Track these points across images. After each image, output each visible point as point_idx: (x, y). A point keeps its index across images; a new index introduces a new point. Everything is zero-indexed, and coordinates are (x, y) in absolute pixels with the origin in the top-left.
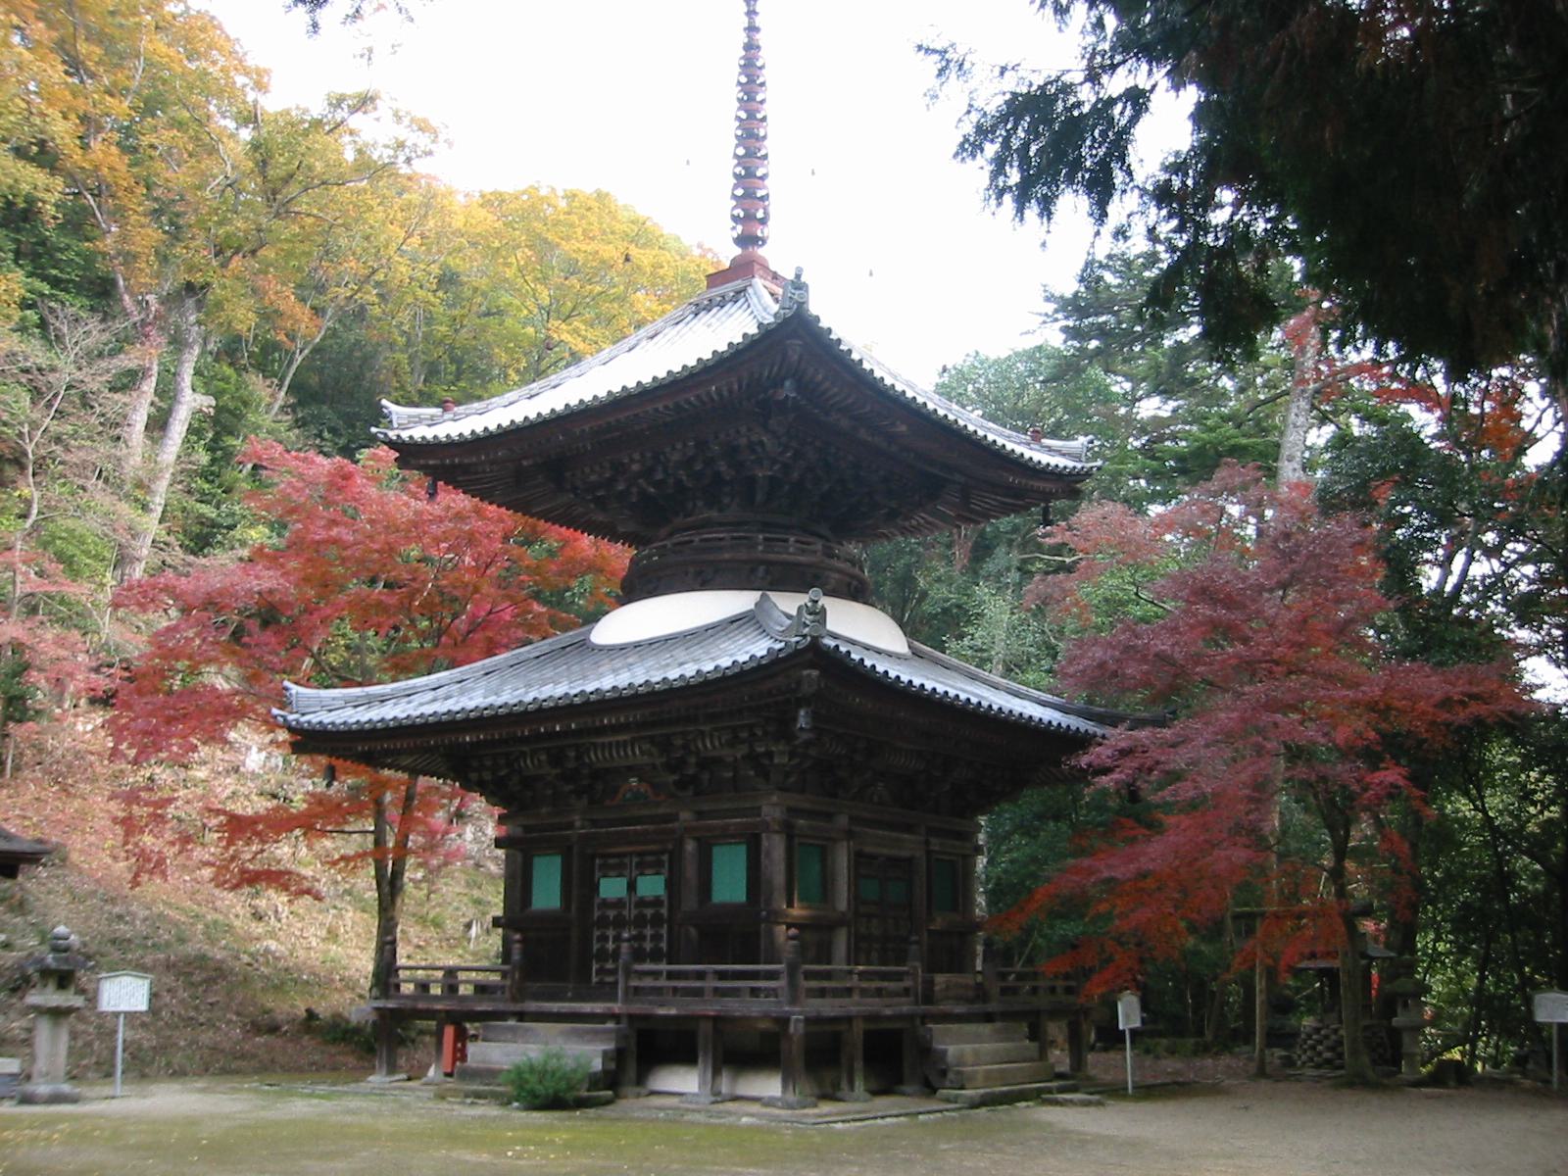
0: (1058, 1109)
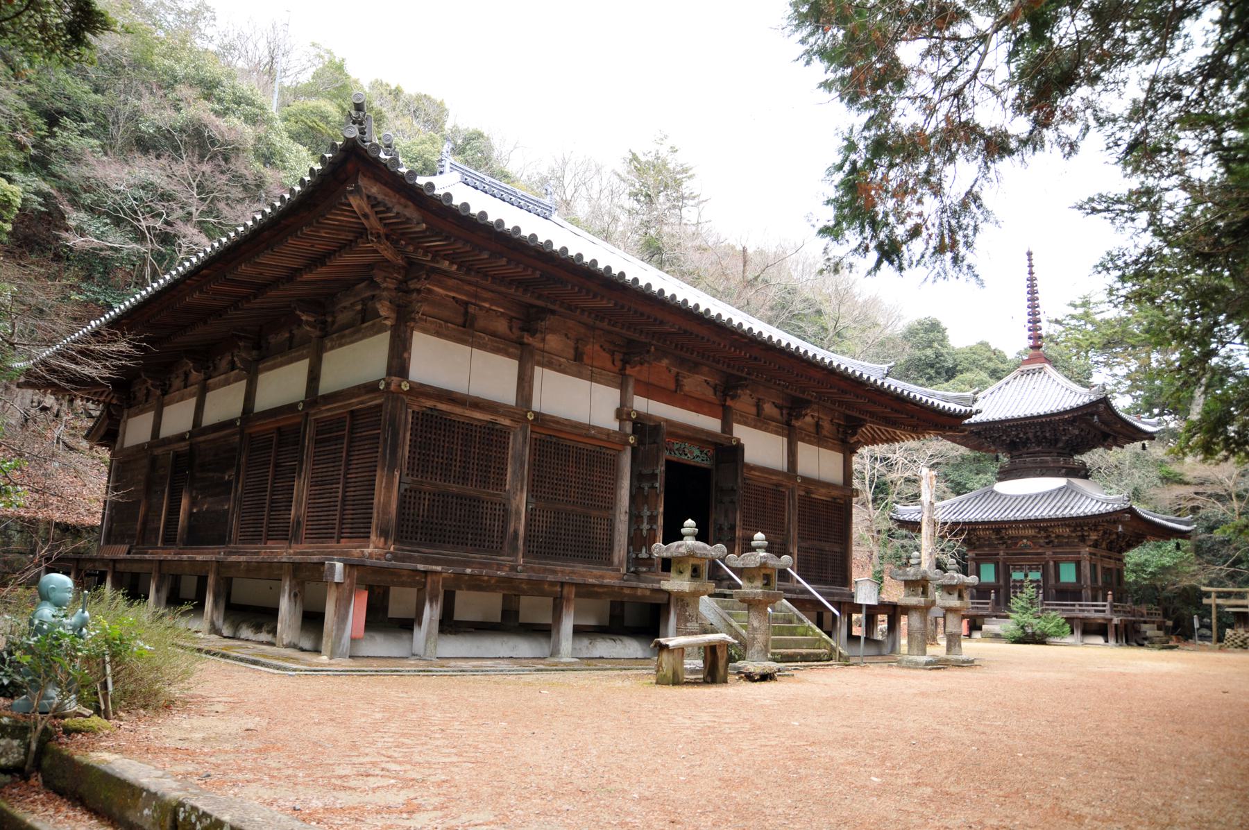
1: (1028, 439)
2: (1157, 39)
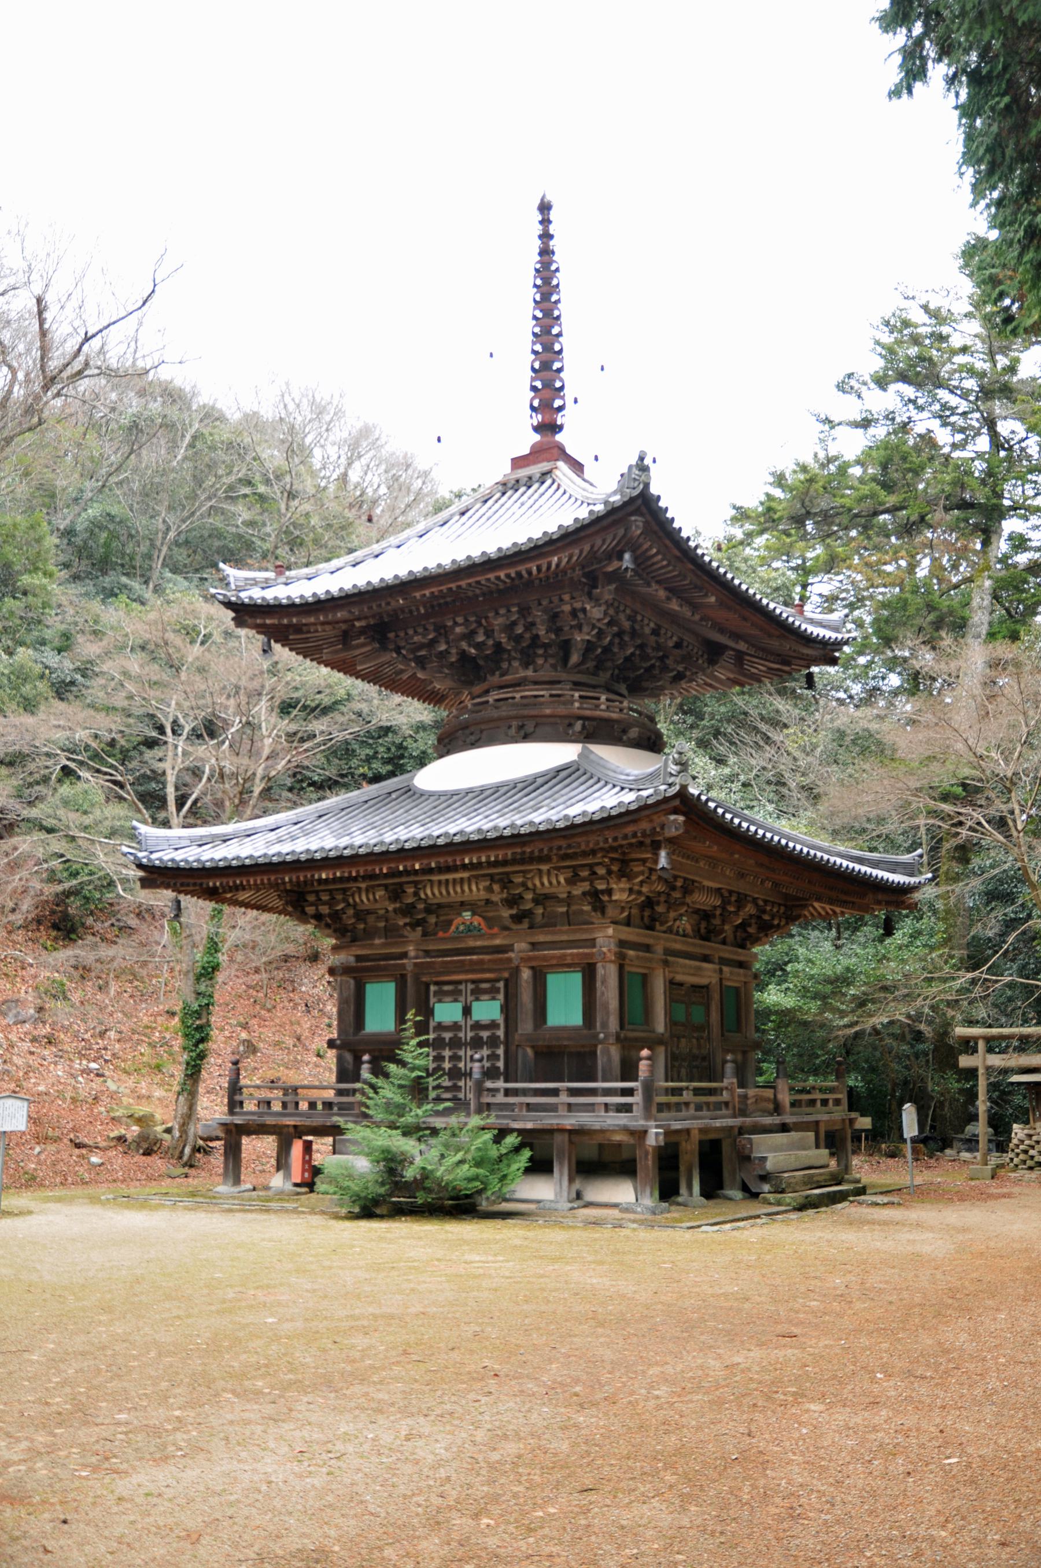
0: (498, 1223)
1: (498, 647)
2: (1017, 305)
